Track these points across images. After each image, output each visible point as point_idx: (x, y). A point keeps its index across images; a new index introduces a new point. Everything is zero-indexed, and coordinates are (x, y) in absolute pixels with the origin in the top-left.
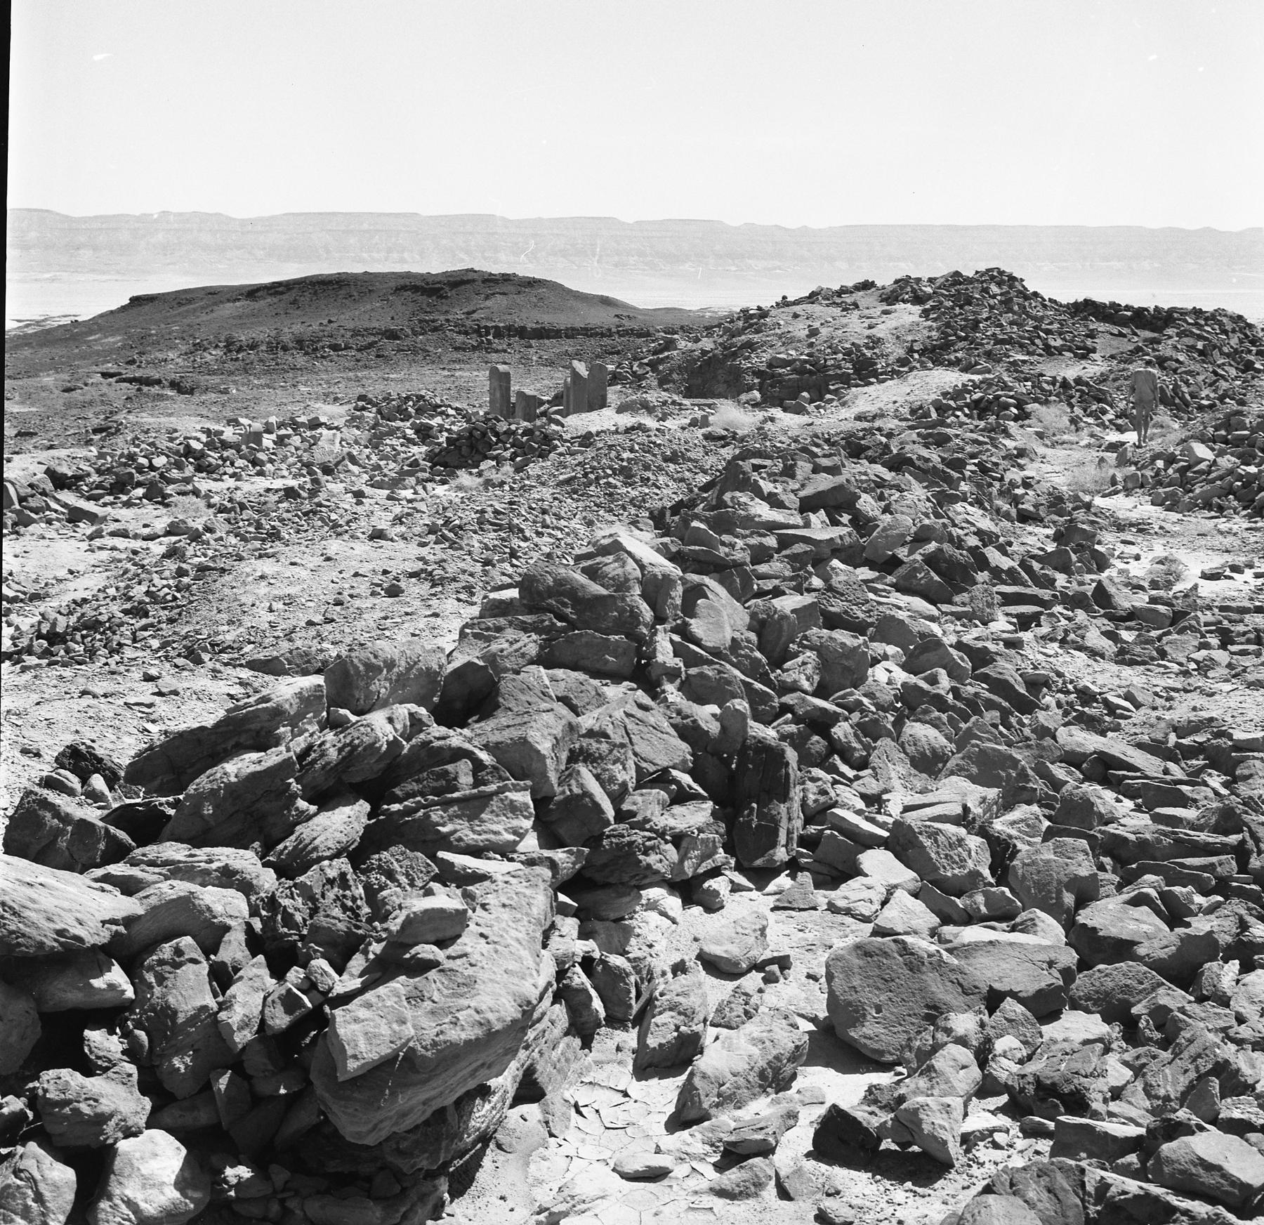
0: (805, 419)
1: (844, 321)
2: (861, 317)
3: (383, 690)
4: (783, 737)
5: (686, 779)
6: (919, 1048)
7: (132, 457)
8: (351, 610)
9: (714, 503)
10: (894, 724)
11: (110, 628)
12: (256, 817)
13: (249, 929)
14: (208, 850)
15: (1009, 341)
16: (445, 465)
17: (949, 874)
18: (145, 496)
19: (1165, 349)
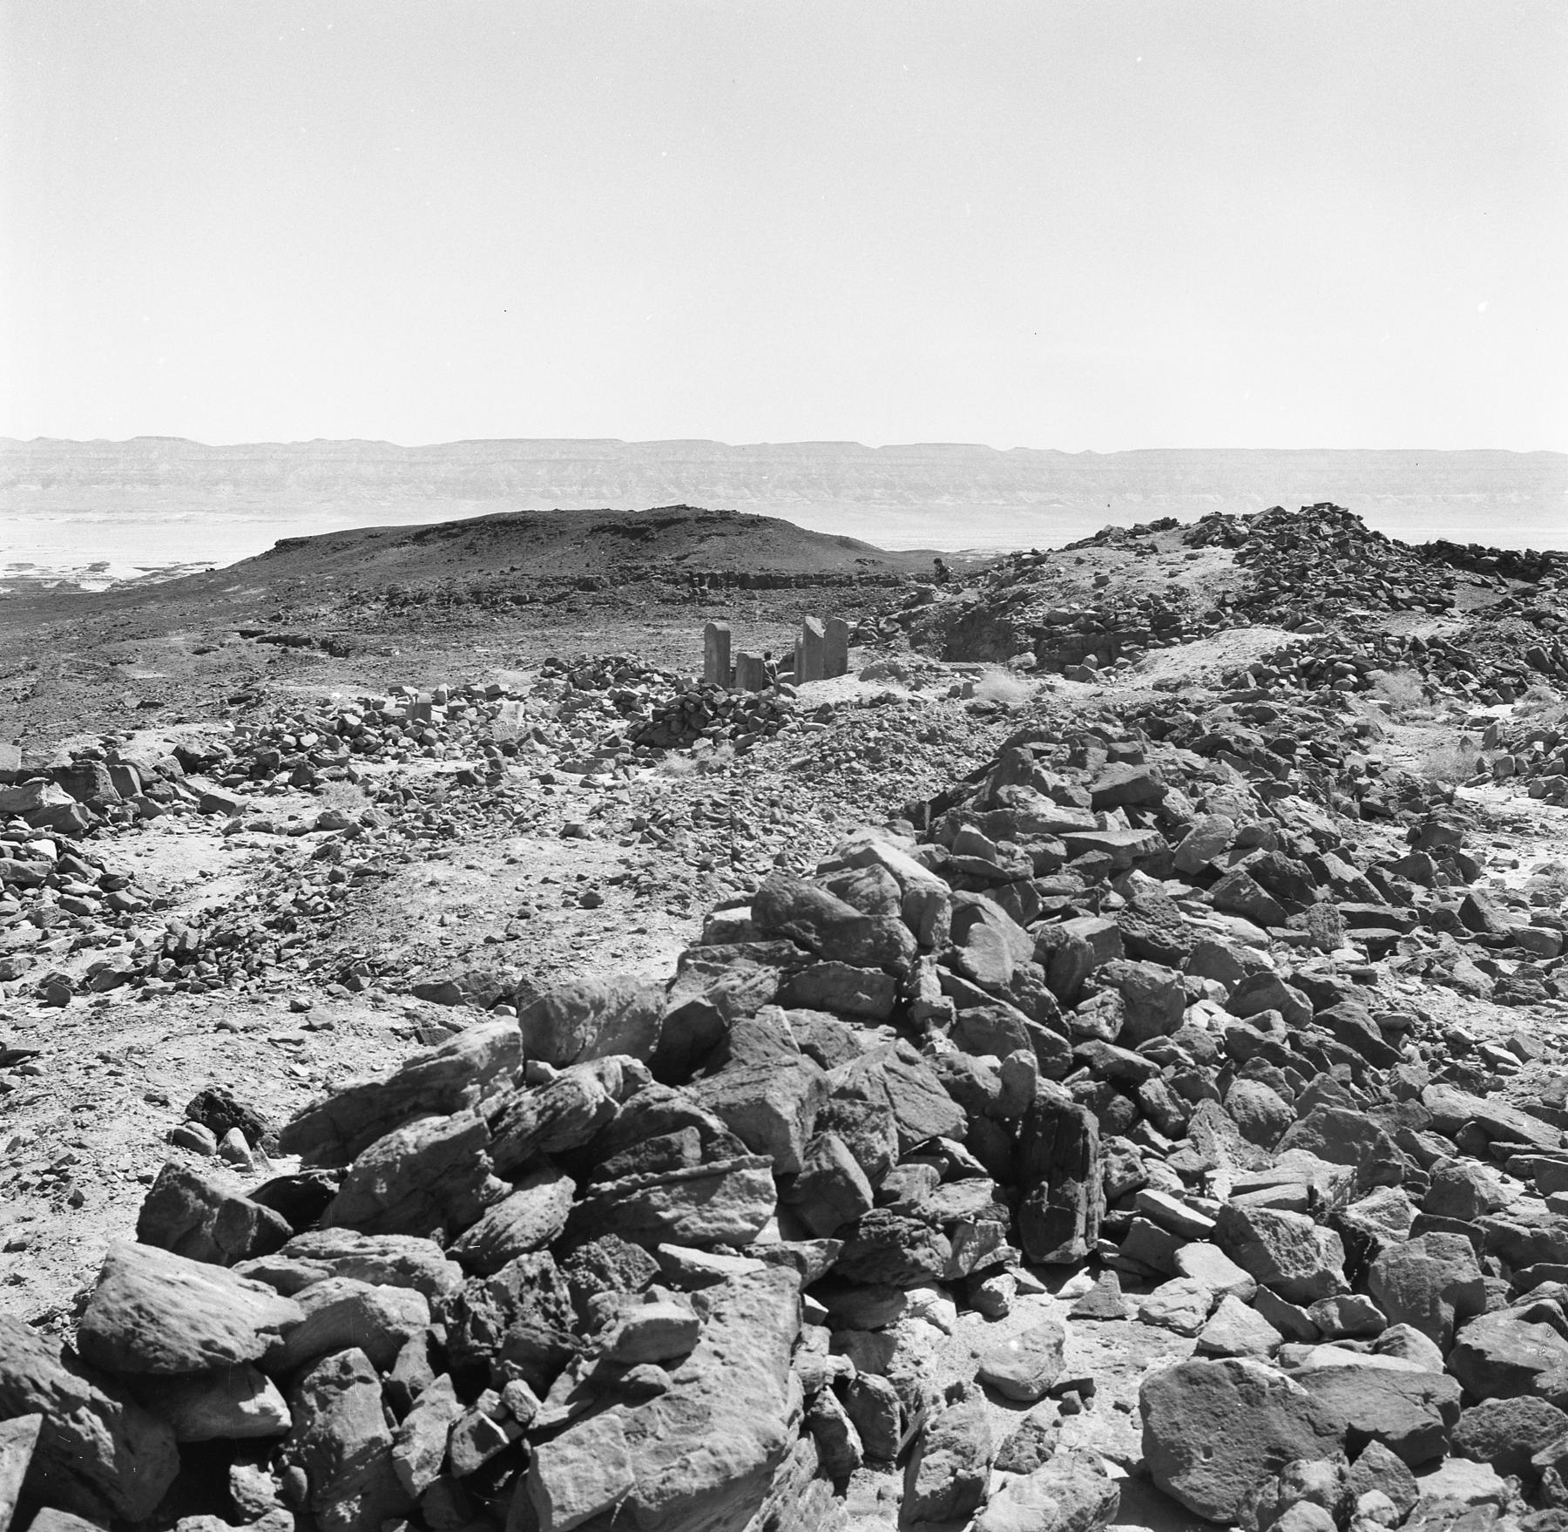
0: (1091, 688)
1: (1140, 567)
2: (1160, 563)
3: (589, 1038)
4: (1079, 1098)
5: (960, 1150)
6: (1261, 1505)
7: (277, 735)
8: (539, 924)
9: (986, 798)
10: (1218, 1081)
11: (249, 945)
12: (439, 1198)
13: (431, 1340)
14: (381, 1238)
15: (1345, 593)
16: (651, 744)
17: (1292, 1276)
18: (291, 782)
19: (1541, 603)
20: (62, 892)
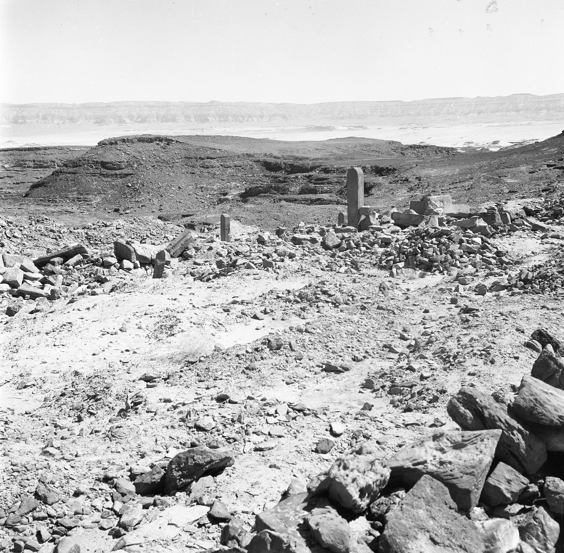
11: (552, 279)
20: (483, 256)
